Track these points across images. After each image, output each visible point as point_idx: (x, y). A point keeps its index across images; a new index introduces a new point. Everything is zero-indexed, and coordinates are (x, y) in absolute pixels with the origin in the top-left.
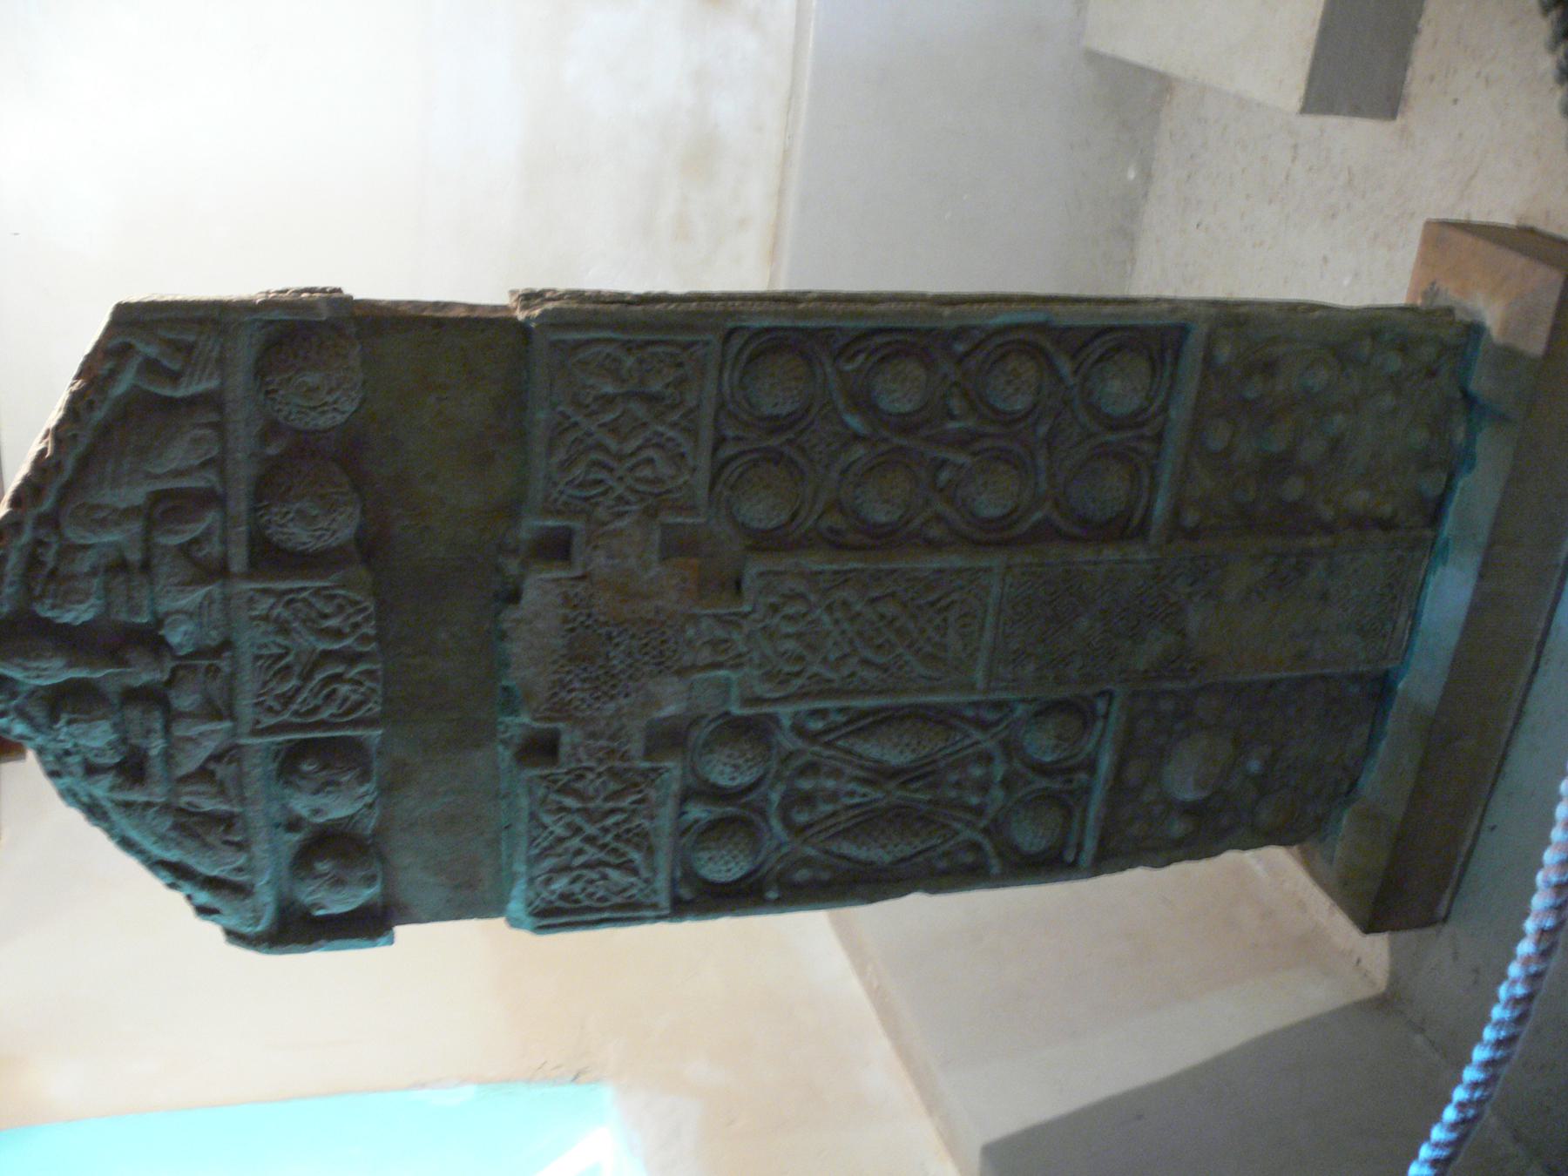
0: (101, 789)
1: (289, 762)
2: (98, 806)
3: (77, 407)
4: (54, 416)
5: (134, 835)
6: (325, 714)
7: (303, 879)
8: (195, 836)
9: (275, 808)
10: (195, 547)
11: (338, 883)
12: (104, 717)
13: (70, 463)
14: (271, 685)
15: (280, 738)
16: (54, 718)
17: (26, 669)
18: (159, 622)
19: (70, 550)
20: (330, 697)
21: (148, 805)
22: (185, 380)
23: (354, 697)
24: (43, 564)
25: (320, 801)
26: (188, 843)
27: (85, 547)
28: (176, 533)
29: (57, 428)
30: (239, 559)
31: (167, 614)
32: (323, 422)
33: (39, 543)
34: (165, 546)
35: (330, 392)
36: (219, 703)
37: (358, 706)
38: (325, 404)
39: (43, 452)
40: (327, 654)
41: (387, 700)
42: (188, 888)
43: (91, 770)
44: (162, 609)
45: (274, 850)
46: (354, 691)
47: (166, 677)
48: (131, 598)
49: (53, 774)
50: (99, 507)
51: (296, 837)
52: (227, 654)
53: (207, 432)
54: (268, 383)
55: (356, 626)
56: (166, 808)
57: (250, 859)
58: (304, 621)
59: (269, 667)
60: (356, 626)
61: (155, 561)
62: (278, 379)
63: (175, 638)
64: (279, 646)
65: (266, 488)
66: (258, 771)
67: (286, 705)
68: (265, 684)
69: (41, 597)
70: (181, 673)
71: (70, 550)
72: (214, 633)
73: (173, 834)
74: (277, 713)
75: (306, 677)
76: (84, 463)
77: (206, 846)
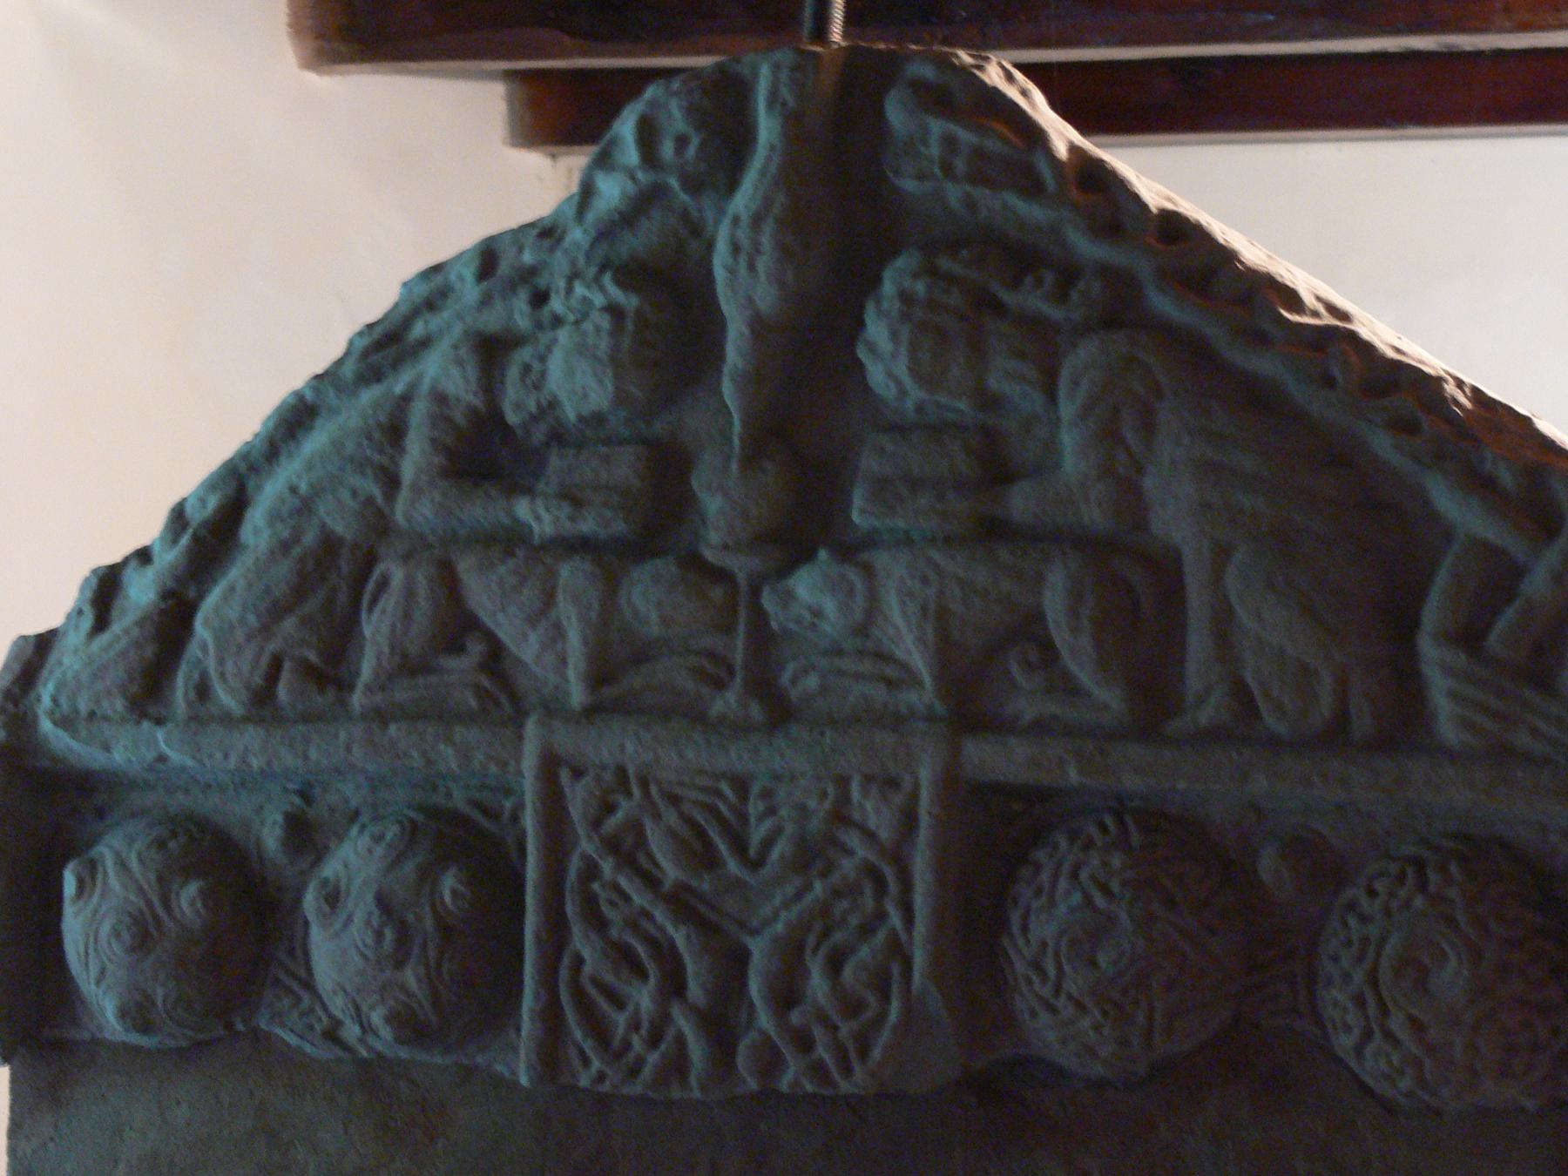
0: (441, 370)
1: (460, 838)
2: (397, 364)
3: (1402, 389)
4: (1381, 330)
5: (316, 441)
6: (583, 943)
7: (161, 844)
8: (300, 592)
9: (351, 792)
10: (1033, 655)
11: (142, 934)
12: (621, 398)
13: (1265, 365)
14: (671, 817)
15: (529, 822)
16: (632, 274)
17: (757, 221)
18: (852, 550)
19: (1044, 349)
20: (626, 958)
21: (391, 481)
22: (1460, 660)
23: (621, 1020)
24: (1015, 283)
25: (361, 907)
26: (284, 570)
27: (1052, 397)
28: (1073, 613)
29: (1353, 337)
30: (993, 759)
31: (868, 570)
32: (1336, 999)
33: (1069, 275)
34: (1040, 578)
35: (1417, 1026)
36: (635, 680)
37: (599, 1030)
38: (1385, 1012)
39: (1292, 299)
40: (738, 959)
41: (603, 1102)
42: (167, 558)
43: (492, 350)
44: (881, 559)
45: (245, 781)
46: (635, 1026)
47: (709, 555)
48: (915, 485)
49: (488, 256)
50: (1148, 426)
51: (271, 837)
52: (756, 712)
53: (1326, 706)
54: (1443, 868)
55: (804, 1043)
56: (379, 524)
57: (227, 719)
58: (825, 910)
59: (712, 811)
60: (804, 1043)
61: (1004, 554)
62: (1452, 893)
63: (806, 585)
64: (768, 843)
65: (1172, 843)
66: (448, 758)
67: (612, 845)
68: (674, 800)
69: (932, 272)
70: (717, 593)
71: (1044, 349)
72: (812, 682)
73: (310, 537)
74: (596, 824)
75: (682, 903)
76: (1258, 399)
77: (276, 612)
